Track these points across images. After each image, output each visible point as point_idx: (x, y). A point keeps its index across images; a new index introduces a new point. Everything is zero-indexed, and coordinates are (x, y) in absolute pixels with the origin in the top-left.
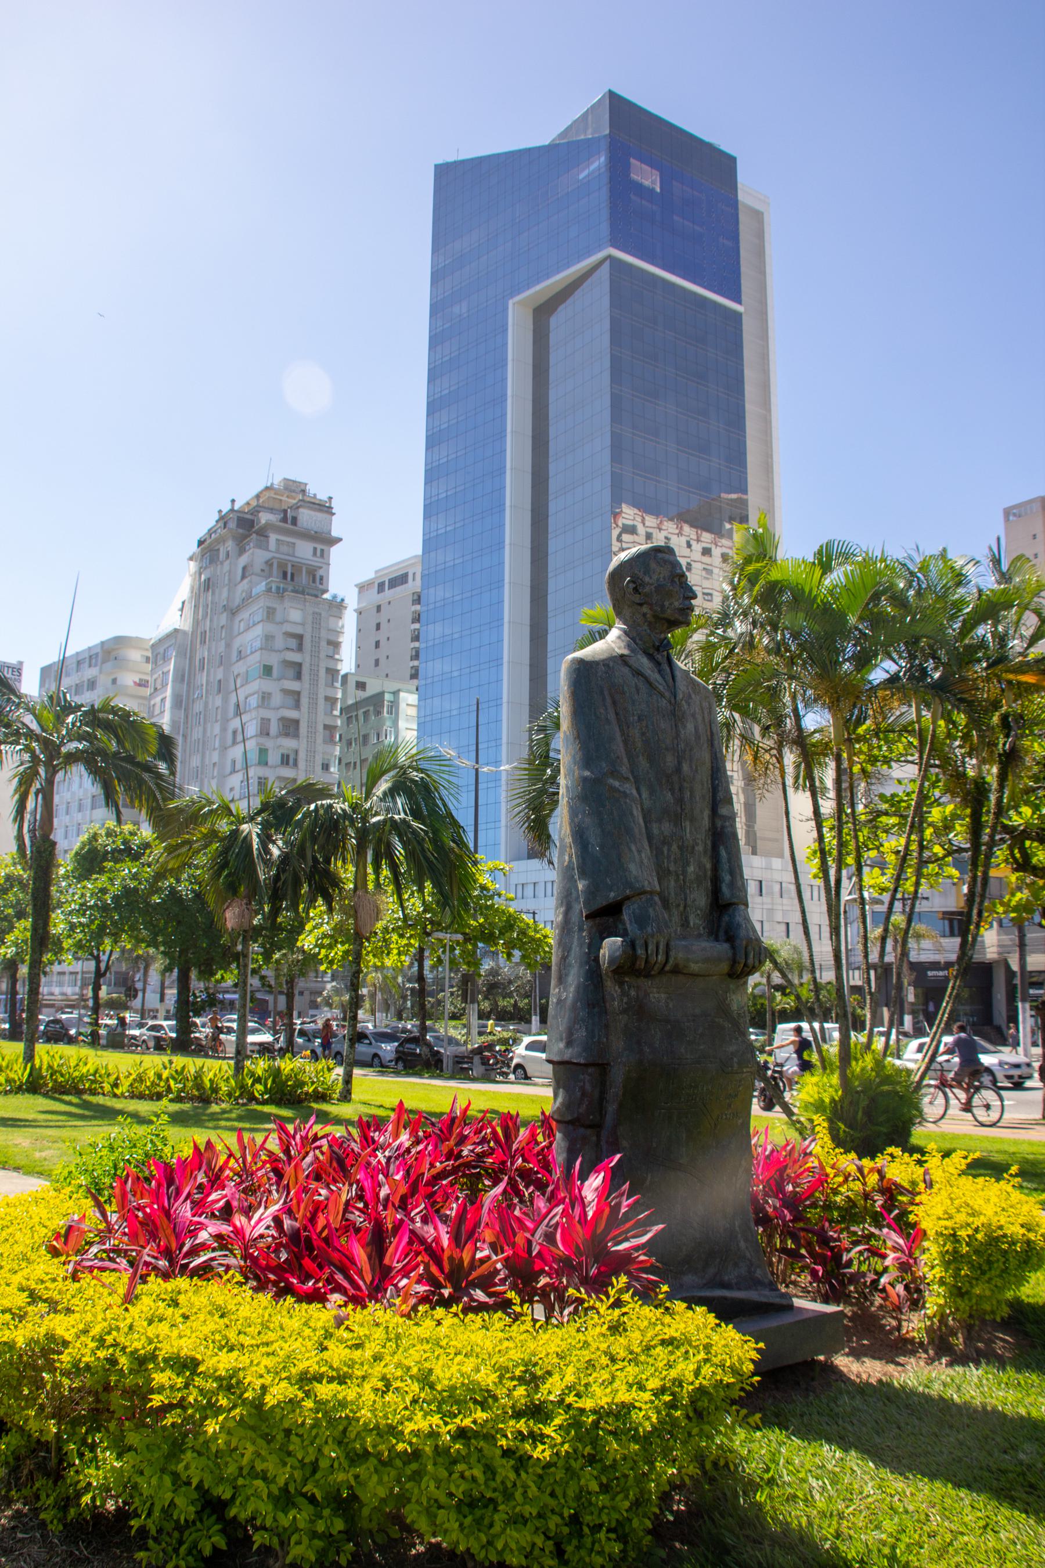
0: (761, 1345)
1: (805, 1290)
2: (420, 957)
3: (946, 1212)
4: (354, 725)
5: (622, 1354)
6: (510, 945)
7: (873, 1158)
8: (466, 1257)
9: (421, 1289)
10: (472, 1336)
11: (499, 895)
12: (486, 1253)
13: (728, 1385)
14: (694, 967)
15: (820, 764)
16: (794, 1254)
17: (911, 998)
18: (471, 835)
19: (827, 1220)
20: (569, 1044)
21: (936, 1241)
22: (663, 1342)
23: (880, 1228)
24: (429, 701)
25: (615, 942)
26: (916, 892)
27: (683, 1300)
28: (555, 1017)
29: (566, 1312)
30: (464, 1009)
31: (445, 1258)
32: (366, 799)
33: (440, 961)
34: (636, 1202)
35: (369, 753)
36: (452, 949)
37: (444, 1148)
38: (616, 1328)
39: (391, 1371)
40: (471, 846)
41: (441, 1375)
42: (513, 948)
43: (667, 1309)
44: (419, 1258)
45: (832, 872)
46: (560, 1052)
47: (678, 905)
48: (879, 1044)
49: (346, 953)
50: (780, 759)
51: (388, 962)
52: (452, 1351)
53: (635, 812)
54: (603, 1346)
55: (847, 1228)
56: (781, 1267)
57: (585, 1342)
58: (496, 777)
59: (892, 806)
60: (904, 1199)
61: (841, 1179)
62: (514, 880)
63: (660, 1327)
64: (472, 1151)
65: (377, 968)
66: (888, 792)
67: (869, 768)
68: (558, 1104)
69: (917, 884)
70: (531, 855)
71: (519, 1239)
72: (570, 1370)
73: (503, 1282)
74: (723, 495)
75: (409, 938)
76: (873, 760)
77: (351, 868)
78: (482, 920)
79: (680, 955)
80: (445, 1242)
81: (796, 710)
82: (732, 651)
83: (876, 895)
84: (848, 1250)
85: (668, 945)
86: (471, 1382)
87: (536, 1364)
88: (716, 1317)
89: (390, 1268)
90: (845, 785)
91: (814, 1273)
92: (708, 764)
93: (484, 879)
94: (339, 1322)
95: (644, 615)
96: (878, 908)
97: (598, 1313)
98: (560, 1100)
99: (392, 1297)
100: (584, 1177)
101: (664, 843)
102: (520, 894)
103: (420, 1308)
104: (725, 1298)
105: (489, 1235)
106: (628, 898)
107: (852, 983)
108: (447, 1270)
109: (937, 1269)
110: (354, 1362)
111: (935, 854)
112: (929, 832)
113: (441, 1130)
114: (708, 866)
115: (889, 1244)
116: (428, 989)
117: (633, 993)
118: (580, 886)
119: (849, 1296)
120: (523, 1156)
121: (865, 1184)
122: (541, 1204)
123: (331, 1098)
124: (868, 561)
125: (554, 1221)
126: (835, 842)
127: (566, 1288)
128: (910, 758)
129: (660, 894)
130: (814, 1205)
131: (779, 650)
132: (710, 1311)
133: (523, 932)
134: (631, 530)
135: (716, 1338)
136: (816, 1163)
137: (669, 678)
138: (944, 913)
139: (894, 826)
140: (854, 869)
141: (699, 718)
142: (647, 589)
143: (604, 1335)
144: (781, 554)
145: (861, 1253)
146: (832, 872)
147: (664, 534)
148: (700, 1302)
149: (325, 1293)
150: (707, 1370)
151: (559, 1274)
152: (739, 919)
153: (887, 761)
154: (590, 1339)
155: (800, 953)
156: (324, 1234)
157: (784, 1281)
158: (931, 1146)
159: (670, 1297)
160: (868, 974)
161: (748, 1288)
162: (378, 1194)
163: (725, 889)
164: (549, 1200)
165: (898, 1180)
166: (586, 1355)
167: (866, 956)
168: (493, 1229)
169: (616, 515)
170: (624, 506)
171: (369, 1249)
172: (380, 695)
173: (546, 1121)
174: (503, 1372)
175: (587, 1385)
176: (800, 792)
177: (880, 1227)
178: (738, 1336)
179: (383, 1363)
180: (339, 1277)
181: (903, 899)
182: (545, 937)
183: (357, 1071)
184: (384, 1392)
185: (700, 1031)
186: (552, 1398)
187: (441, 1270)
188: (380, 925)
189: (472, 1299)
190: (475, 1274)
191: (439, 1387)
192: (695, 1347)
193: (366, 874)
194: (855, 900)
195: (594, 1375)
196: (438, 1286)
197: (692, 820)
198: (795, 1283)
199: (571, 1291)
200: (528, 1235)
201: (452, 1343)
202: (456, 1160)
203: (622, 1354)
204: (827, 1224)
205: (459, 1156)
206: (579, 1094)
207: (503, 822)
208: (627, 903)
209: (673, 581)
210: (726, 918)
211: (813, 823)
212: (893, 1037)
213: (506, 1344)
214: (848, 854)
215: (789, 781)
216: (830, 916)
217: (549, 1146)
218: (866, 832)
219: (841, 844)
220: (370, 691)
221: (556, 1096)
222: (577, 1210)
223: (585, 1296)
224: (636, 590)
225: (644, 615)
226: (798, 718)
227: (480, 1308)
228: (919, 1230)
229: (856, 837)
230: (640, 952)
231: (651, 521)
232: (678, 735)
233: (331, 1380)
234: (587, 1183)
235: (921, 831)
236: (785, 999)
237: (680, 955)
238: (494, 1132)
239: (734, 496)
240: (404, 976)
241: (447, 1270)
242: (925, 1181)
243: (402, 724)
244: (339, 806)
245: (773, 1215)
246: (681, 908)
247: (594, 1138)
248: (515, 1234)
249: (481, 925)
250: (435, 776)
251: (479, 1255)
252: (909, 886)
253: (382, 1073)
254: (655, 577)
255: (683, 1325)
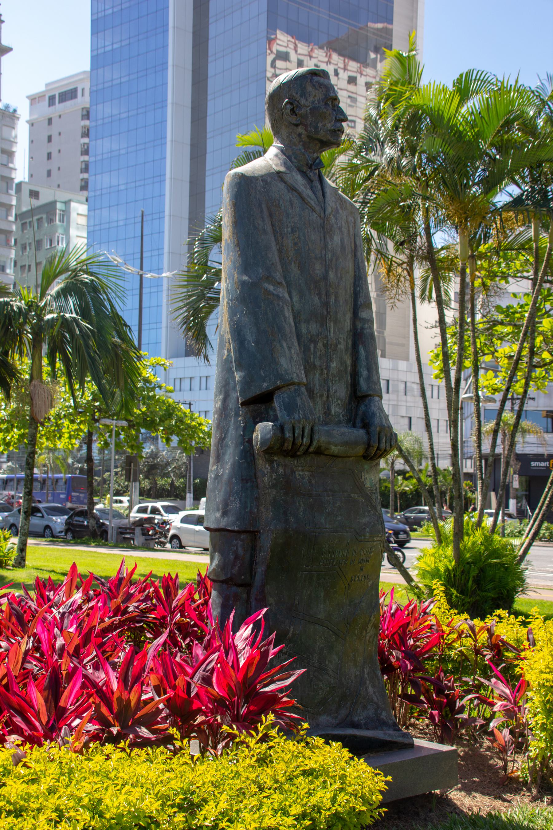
0: (389, 778)
1: (422, 731)
2: (88, 441)
3: (547, 667)
4: (28, 229)
5: (269, 782)
6: (169, 432)
7: (483, 619)
8: (133, 698)
9: (91, 727)
10: (138, 769)
11: (160, 387)
12: (150, 695)
13: (360, 813)
14: (335, 449)
15: (444, 278)
16: (414, 700)
17: (516, 484)
18: (136, 334)
19: (442, 671)
20: (225, 513)
21: (538, 691)
22: (305, 773)
23: (488, 678)
24: (98, 212)
25: (266, 426)
26: (525, 392)
27: (321, 736)
28: (213, 491)
29: (220, 746)
30: (127, 487)
31: (115, 699)
32: (41, 299)
33: (106, 444)
34: (280, 651)
35: (43, 258)
36: (118, 434)
37: (112, 605)
38: (263, 761)
39: (63, 802)
40: (136, 343)
41: (110, 804)
42: (171, 434)
43: (307, 743)
44: (91, 700)
45: (453, 373)
46: (217, 521)
47: (321, 396)
48: (488, 522)
49: (22, 436)
50: (410, 273)
51: (60, 445)
52: (120, 782)
53: (287, 313)
54: (252, 776)
55: (460, 679)
56: (402, 711)
57: (237, 772)
58: (158, 282)
59: (507, 316)
60: (509, 655)
61: (455, 636)
62: (173, 374)
63: (301, 759)
64: (137, 607)
65: (50, 450)
66: (504, 304)
67: (489, 282)
68: (214, 566)
69: (527, 385)
70: (189, 352)
71: (180, 682)
72: (224, 797)
73: (164, 719)
74: (370, 25)
75: (79, 424)
76: (492, 275)
77: (27, 361)
78: (144, 409)
79: (323, 439)
80: (115, 686)
81: (427, 229)
82: (372, 173)
83: (489, 394)
84: (462, 698)
85: (312, 430)
86: (137, 810)
87: (193, 793)
88: (350, 751)
89: (65, 709)
90: (467, 297)
91: (432, 718)
92: (351, 273)
93: (147, 373)
94: (17, 760)
95: (300, 135)
96: (491, 406)
97: (248, 747)
98: (215, 562)
99: (66, 735)
100: (236, 629)
101: (311, 341)
102: (178, 387)
103: (91, 745)
104: (355, 736)
105: (153, 680)
106: (278, 388)
107: (465, 470)
108: (116, 710)
109: (539, 716)
110: (30, 796)
111: (543, 360)
112: (539, 340)
113: (110, 589)
114: (349, 362)
115: (496, 693)
116: (96, 469)
117: (281, 470)
118: (237, 377)
119: (461, 738)
120: (180, 611)
121: (476, 641)
122: (199, 651)
123: (7, 565)
124: (503, 90)
125: (210, 667)
126: (456, 347)
127: (220, 726)
128: (525, 274)
129: (306, 385)
130: (431, 658)
131: (415, 172)
132: (344, 746)
133: (180, 420)
134: (284, 57)
135: (350, 770)
136: (434, 622)
137: (320, 194)
138: (547, 411)
139: (508, 334)
140: (471, 370)
141: (345, 230)
142: (303, 111)
143: (252, 766)
144: (424, 82)
145: (471, 700)
146: (453, 373)
147: (314, 61)
148: (336, 738)
149: (4, 735)
150: (342, 798)
151: (214, 712)
152: (374, 409)
153: (505, 277)
154: (241, 770)
155: (420, 444)
156: (4, 682)
157: (404, 724)
158: (534, 611)
159: (310, 733)
160: (481, 462)
161: (375, 728)
162: (54, 645)
163: (363, 383)
164: (206, 648)
165: (505, 638)
166: (238, 784)
167: (479, 446)
168: (158, 673)
169: (270, 41)
170: (278, 32)
171: (46, 693)
172: (54, 203)
173: (201, 582)
174: (164, 799)
175: (238, 811)
176: (426, 302)
177: (488, 678)
178: (369, 769)
179: (57, 796)
180: (18, 720)
181: (513, 399)
182: (200, 424)
183: (31, 541)
184: (57, 822)
185: (338, 504)
186: (207, 823)
187: (111, 710)
188: (53, 412)
189: (137, 736)
190: (140, 714)
191: (108, 816)
192: (332, 777)
193: (41, 366)
194: (471, 398)
195: (245, 802)
196: (107, 724)
197: (336, 322)
198: (414, 725)
199: (225, 727)
200: (187, 678)
201: (119, 775)
202: (122, 616)
203: (269, 783)
204: (442, 674)
205: (125, 612)
206: (232, 557)
207: (164, 324)
208: (278, 392)
209: (326, 104)
210: (362, 408)
211: (438, 330)
212: (500, 518)
213: (168, 775)
214: (466, 358)
215: (417, 293)
216: (449, 410)
217: (206, 602)
218: (482, 339)
219: (462, 349)
220: (44, 199)
221: (212, 559)
222: (231, 657)
223: (237, 732)
224: (293, 111)
225: (300, 135)
226: (429, 236)
227: (143, 743)
228: (523, 681)
229: (475, 343)
230: (288, 435)
231: (303, 48)
232: (326, 246)
233: (9, 813)
234: (238, 634)
235: (533, 339)
236: (406, 482)
237: (323, 439)
238: (156, 591)
239: (380, 26)
240: (74, 458)
241: (116, 710)
242: (528, 640)
243: (73, 232)
244: (17, 304)
245: (396, 666)
246: (324, 398)
247: (245, 596)
248: (176, 678)
249: (143, 413)
250: (104, 280)
251: (144, 697)
252: (518, 387)
253: (53, 543)
254: (310, 99)
255: (321, 758)
